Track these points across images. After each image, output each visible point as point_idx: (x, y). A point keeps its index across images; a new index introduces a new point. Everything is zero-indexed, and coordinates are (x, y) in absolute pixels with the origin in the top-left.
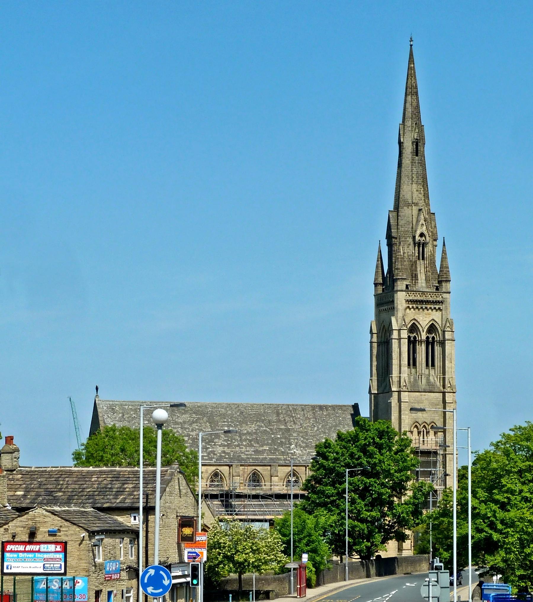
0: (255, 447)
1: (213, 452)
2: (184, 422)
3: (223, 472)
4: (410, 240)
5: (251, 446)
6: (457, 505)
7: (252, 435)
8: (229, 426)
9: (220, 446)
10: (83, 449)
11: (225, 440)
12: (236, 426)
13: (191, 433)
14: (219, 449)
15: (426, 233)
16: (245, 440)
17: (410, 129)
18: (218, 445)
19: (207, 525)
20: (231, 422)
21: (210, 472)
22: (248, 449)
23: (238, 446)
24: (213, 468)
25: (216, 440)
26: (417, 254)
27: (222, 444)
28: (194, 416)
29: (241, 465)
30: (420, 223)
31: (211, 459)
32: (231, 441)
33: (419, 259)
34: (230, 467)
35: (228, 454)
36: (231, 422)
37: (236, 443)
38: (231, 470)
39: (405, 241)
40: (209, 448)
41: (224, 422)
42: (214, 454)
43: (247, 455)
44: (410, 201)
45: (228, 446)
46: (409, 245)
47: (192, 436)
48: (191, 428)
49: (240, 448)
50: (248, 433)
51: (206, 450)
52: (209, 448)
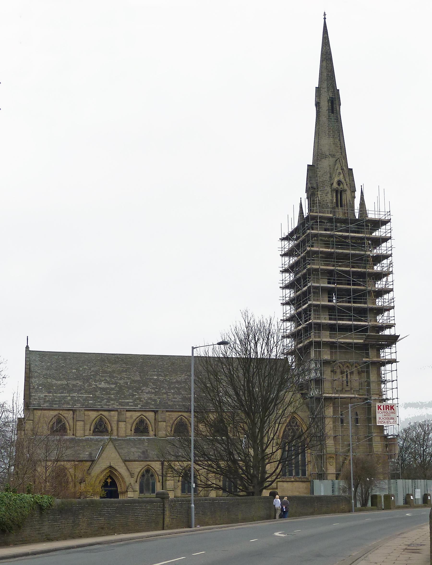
0: (183, 394)
1: (139, 399)
2: (114, 372)
3: (149, 418)
4: (328, 189)
5: (180, 394)
6: (91, 438)
7: (181, 384)
8: (158, 375)
9: (147, 393)
10: (33, 396)
11: (153, 388)
12: (166, 375)
13: (120, 382)
14: (146, 396)
15: (343, 180)
16: (173, 388)
17: (326, 90)
18: (145, 392)
19: (114, 466)
20: (161, 372)
21: (134, 418)
22: (175, 396)
23: (166, 393)
24: (138, 414)
25: (144, 388)
26: (335, 201)
27: (149, 391)
28: (124, 365)
29: (167, 411)
30: (338, 172)
31: (136, 405)
32: (160, 389)
33: (337, 206)
34: (155, 413)
35: (155, 400)
36: (161, 372)
37: (164, 391)
38: (157, 416)
39: (324, 190)
40: (136, 395)
41: (154, 371)
42: (140, 401)
43: (174, 402)
44: (327, 153)
45: (156, 393)
46: (327, 193)
47: (120, 384)
48: (119, 377)
49: (168, 395)
50: (177, 382)
51: (132, 397)
52: (136, 395)
